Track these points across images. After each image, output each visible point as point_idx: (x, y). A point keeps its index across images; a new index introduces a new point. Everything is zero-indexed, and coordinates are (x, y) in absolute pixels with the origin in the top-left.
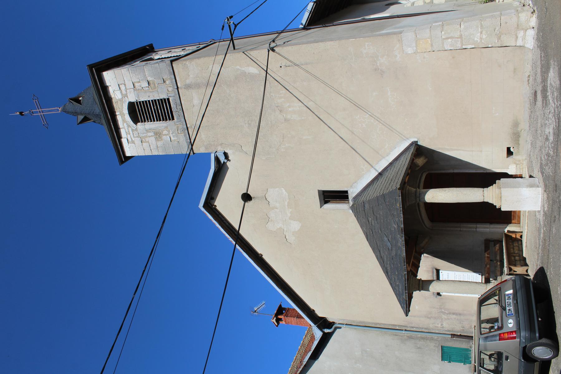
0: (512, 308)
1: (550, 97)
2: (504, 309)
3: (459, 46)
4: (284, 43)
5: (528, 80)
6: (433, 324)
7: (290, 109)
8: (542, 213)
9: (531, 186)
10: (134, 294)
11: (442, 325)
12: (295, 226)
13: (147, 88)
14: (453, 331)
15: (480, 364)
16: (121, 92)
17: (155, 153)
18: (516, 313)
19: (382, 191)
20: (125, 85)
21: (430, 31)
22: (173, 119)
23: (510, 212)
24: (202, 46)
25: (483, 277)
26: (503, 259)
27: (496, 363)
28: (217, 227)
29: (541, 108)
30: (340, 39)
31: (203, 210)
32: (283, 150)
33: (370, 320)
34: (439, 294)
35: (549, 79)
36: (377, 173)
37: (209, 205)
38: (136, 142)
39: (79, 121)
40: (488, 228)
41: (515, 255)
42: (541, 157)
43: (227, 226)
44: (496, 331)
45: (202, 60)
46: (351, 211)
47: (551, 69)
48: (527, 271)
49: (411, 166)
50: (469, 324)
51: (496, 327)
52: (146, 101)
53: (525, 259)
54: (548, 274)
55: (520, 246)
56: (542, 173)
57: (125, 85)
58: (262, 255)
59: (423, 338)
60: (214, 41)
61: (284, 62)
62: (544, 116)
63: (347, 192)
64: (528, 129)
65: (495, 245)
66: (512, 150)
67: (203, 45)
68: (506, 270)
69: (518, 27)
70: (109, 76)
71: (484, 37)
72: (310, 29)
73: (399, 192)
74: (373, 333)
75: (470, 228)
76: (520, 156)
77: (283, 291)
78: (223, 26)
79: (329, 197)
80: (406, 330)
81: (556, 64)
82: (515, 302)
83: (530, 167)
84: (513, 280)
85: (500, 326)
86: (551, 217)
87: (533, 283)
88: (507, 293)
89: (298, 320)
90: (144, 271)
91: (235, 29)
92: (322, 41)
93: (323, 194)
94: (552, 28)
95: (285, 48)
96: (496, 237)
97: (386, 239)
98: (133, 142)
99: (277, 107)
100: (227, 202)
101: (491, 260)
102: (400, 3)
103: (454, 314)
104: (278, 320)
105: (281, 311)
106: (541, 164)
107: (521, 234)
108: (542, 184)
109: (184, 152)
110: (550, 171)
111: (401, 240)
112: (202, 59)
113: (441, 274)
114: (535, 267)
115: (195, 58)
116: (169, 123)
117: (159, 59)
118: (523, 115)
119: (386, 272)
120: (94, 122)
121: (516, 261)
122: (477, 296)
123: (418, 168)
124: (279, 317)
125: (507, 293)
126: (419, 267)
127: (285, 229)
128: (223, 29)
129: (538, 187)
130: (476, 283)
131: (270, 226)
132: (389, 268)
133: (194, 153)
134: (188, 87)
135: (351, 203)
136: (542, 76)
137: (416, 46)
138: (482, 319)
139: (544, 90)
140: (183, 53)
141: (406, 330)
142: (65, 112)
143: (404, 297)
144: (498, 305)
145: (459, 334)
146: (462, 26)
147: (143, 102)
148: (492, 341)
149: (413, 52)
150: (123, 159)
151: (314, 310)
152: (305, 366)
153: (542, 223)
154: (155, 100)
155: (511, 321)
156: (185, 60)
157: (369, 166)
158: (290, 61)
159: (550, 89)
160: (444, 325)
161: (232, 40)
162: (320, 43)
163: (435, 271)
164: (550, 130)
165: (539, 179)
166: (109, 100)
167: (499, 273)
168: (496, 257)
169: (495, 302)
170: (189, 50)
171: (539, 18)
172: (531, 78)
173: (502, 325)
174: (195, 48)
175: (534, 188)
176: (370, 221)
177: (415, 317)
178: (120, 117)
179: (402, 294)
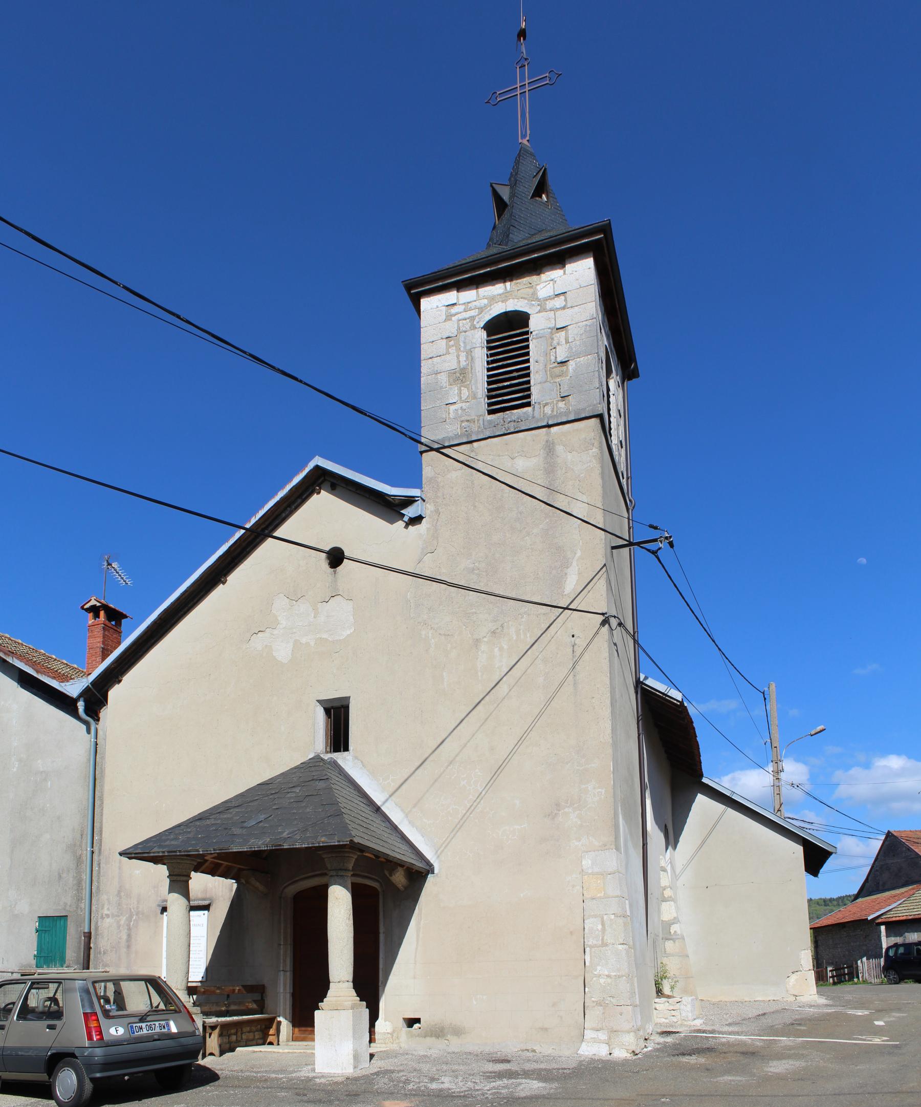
0: (145, 1031)
1: (499, 1083)
2: (143, 1018)
3: (590, 941)
4: (615, 644)
5: (528, 1050)
6: (108, 899)
7: (496, 650)
8: (311, 1075)
9: (356, 1057)
10: (125, 288)
11: (108, 916)
12: (283, 652)
13: (553, 358)
14: (97, 935)
15: (38, 983)
16: (550, 298)
17: (425, 367)
18: (135, 1038)
19: (349, 812)
20: (564, 308)
21: (617, 896)
22: (491, 412)
23: (312, 1025)
24: (624, 482)
25: (199, 984)
26: (230, 1016)
27: (41, 1009)
28: (276, 494)
29: (482, 1069)
30: (615, 744)
31: (311, 465)
32: (423, 633)
33: (107, 788)
34: (164, 909)
35: (528, 1081)
36: (379, 803)
37: (320, 480)
38: (449, 323)
39: (498, 188)
40: (285, 989)
41: (239, 1034)
42: (403, 1071)
43: (280, 514)
44: (102, 1007)
45: (598, 482)
46: (311, 756)
47: (543, 1085)
48: (211, 1054)
49: (391, 862)
50: (111, 961)
51: (107, 1007)
52: (528, 354)
53: (232, 1050)
54: (208, 1087)
55: (254, 1042)
56: (377, 1074)
57: (564, 308)
58: (224, 583)
59: (79, 883)
60: (631, 508)
61: (581, 642)
62: (470, 1075)
63: (346, 749)
64: (450, 1051)
65: (255, 1001)
66: (416, 1026)
67: (627, 485)
68: (213, 1020)
69: (613, 1032)
70: (582, 272)
71: (602, 981)
72: (636, 693)
73: (346, 841)
74: (82, 793)
75: (285, 961)
76: (406, 1040)
77: (155, 623)
78: (656, 528)
79: (338, 715)
80: (93, 852)
81: (552, 1091)
82: (156, 1037)
83: (387, 1055)
84: (194, 1032)
85: (111, 1014)
86: (305, 1089)
87: (190, 1065)
88: (172, 1024)
89: (99, 651)
90: (178, 317)
91: (649, 550)
92: (613, 713)
93: (342, 706)
94: (608, 1081)
95: (606, 645)
96: (269, 1002)
97: (262, 817)
98: (449, 317)
99: (502, 626)
100: (326, 517)
101: (228, 996)
102: (667, 849)
103: (129, 936)
104: (95, 610)
105: (115, 616)
106: (392, 1072)
107: (275, 1043)
108: (359, 1073)
109: (424, 432)
110: (381, 1085)
111: (260, 843)
112: (600, 481)
113: (202, 912)
114: (218, 1067)
115: (602, 467)
116: (483, 402)
117: (608, 390)
118: (471, 1043)
119: (201, 817)
120: (494, 228)
121: (229, 1036)
122: (163, 974)
123: (387, 873)
124: (102, 613)
125: (172, 1024)
126: (213, 875)
127: (275, 632)
128: (651, 526)
129: (355, 1067)
130: (188, 972)
131: (281, 603)
132: (208, 822)
133: (422, 453)
134: (550, 449)
135: (327, 757)
136: (534, 1071)
137: (593, 874)
138: (122, 983)
139: (511, 1074)
140: (614, 441)
141: (93, 852)
142: (519, 155)
143: (156, 849)
144: (149, 1008)
145: (92, 945)
146: (620, 947)
147: (527, 347)
148: (82, 1000)
149: (584, 868)
150: (418, 289)
151: (120, 681)
152: (5, 661)
153: (294, 1075)
154: (528, 375)
155: (121, 1031)
156: (601, 448)
157: (392, 790)
158: (582, 654)
159: (512, 1084)
160: (108, 921)
161: (630, 544)
162: (609, 711)
163: (206, 903)
164: (447, 1083)
165: (367, 1068)
166: (536, 267)
167: (206, 1009)
168: (235, 1004)
169: (155, 1005)
170: (620, 455)
171: (625, 1062)
172: (530, 1054)
173: (113, 1017)
174: (622, 467)
175: (352, 1061)
176: (294, 790)
177: (120, 868)
178: (501, 291)
179: (160, 846)
